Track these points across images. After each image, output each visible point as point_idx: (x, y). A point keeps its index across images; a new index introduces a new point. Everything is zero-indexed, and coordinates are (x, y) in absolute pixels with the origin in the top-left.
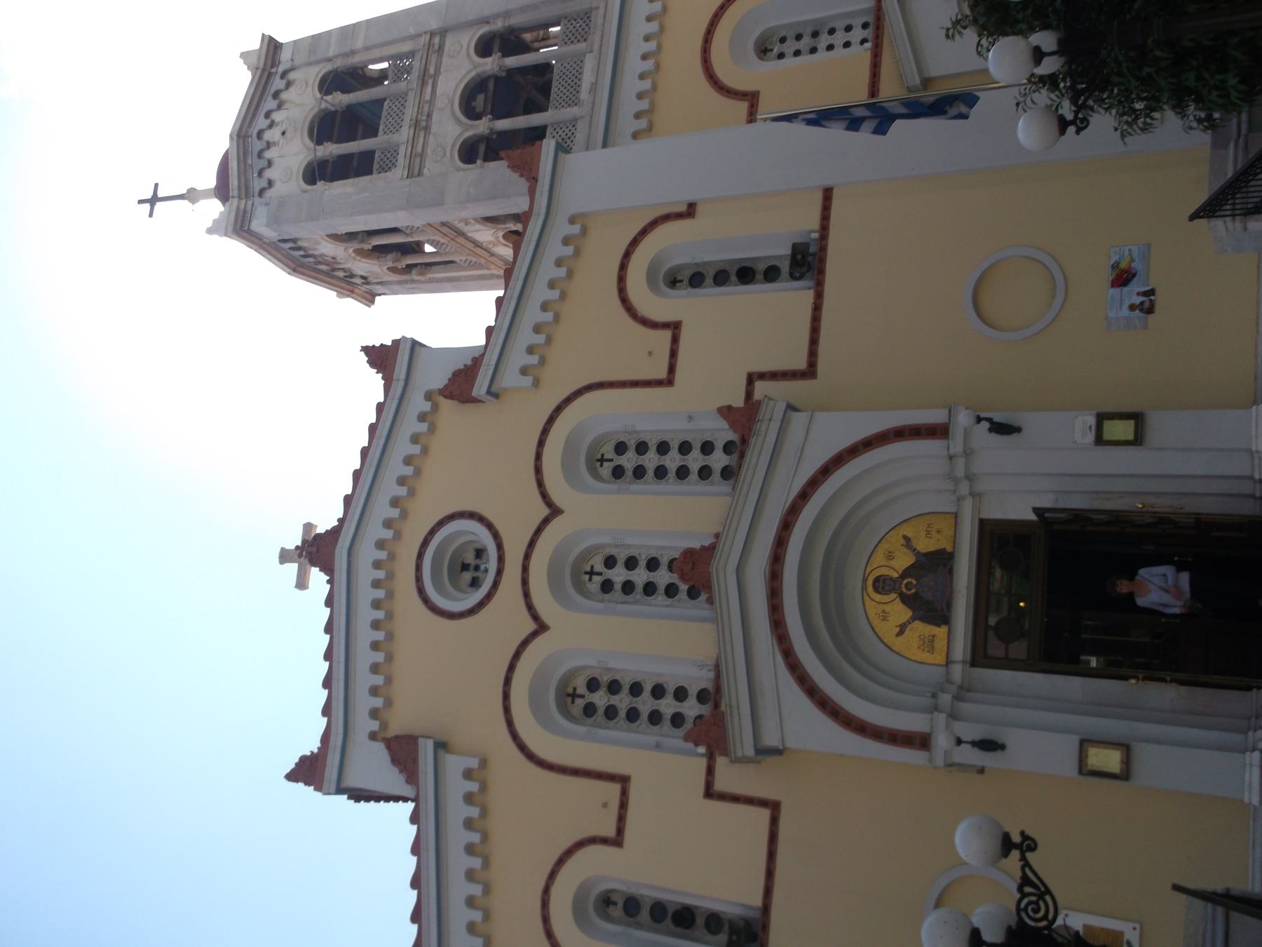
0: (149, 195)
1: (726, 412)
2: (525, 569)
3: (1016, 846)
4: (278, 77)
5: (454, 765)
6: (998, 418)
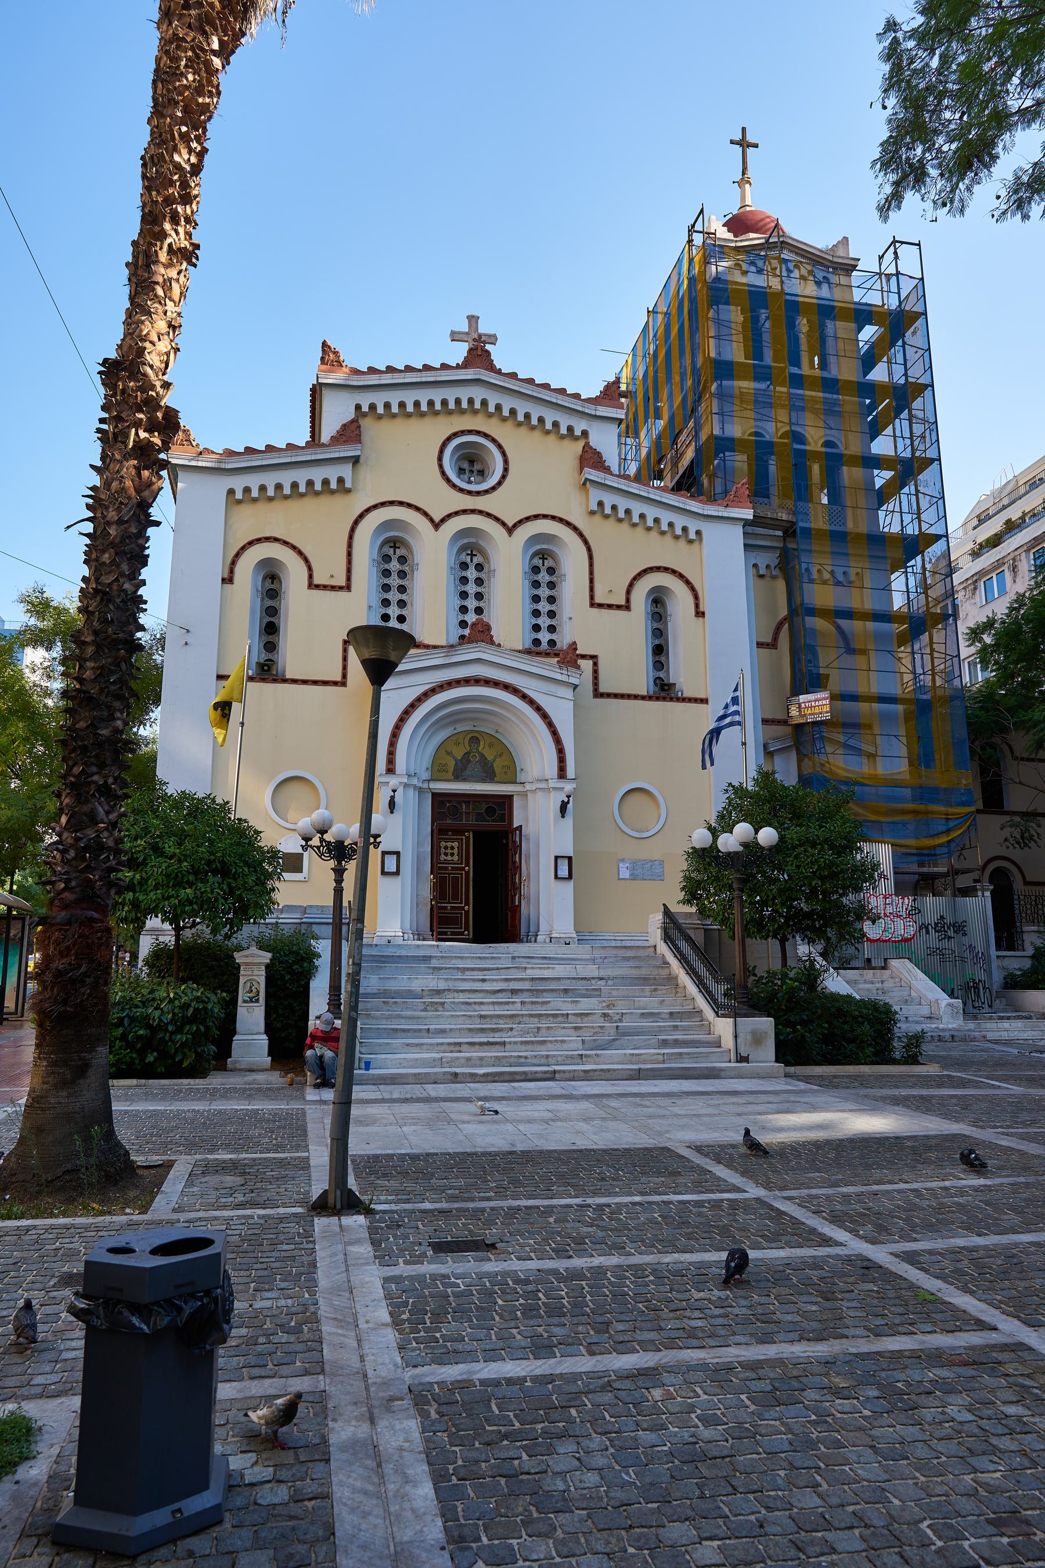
0: (750, 138)
1: (573, 646)
2: (473, 511)
4: (825, 274)
5: (345, 471)
6: (570, 806)
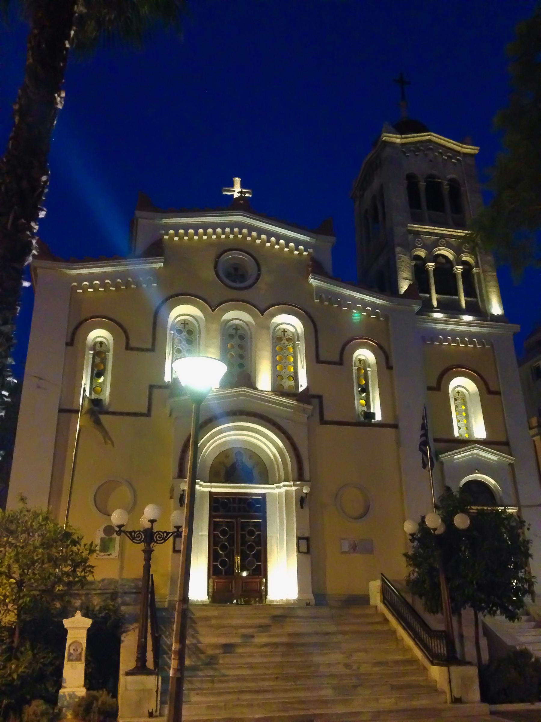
3: (178, 530)
